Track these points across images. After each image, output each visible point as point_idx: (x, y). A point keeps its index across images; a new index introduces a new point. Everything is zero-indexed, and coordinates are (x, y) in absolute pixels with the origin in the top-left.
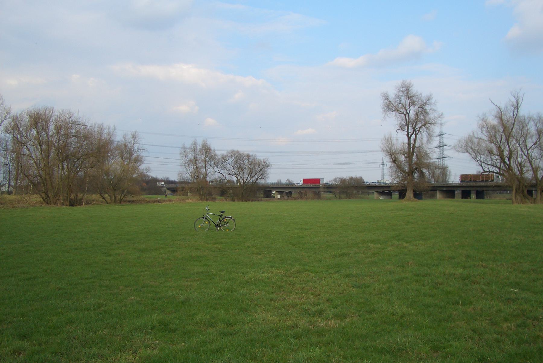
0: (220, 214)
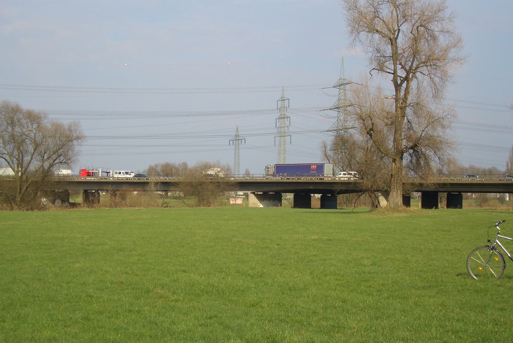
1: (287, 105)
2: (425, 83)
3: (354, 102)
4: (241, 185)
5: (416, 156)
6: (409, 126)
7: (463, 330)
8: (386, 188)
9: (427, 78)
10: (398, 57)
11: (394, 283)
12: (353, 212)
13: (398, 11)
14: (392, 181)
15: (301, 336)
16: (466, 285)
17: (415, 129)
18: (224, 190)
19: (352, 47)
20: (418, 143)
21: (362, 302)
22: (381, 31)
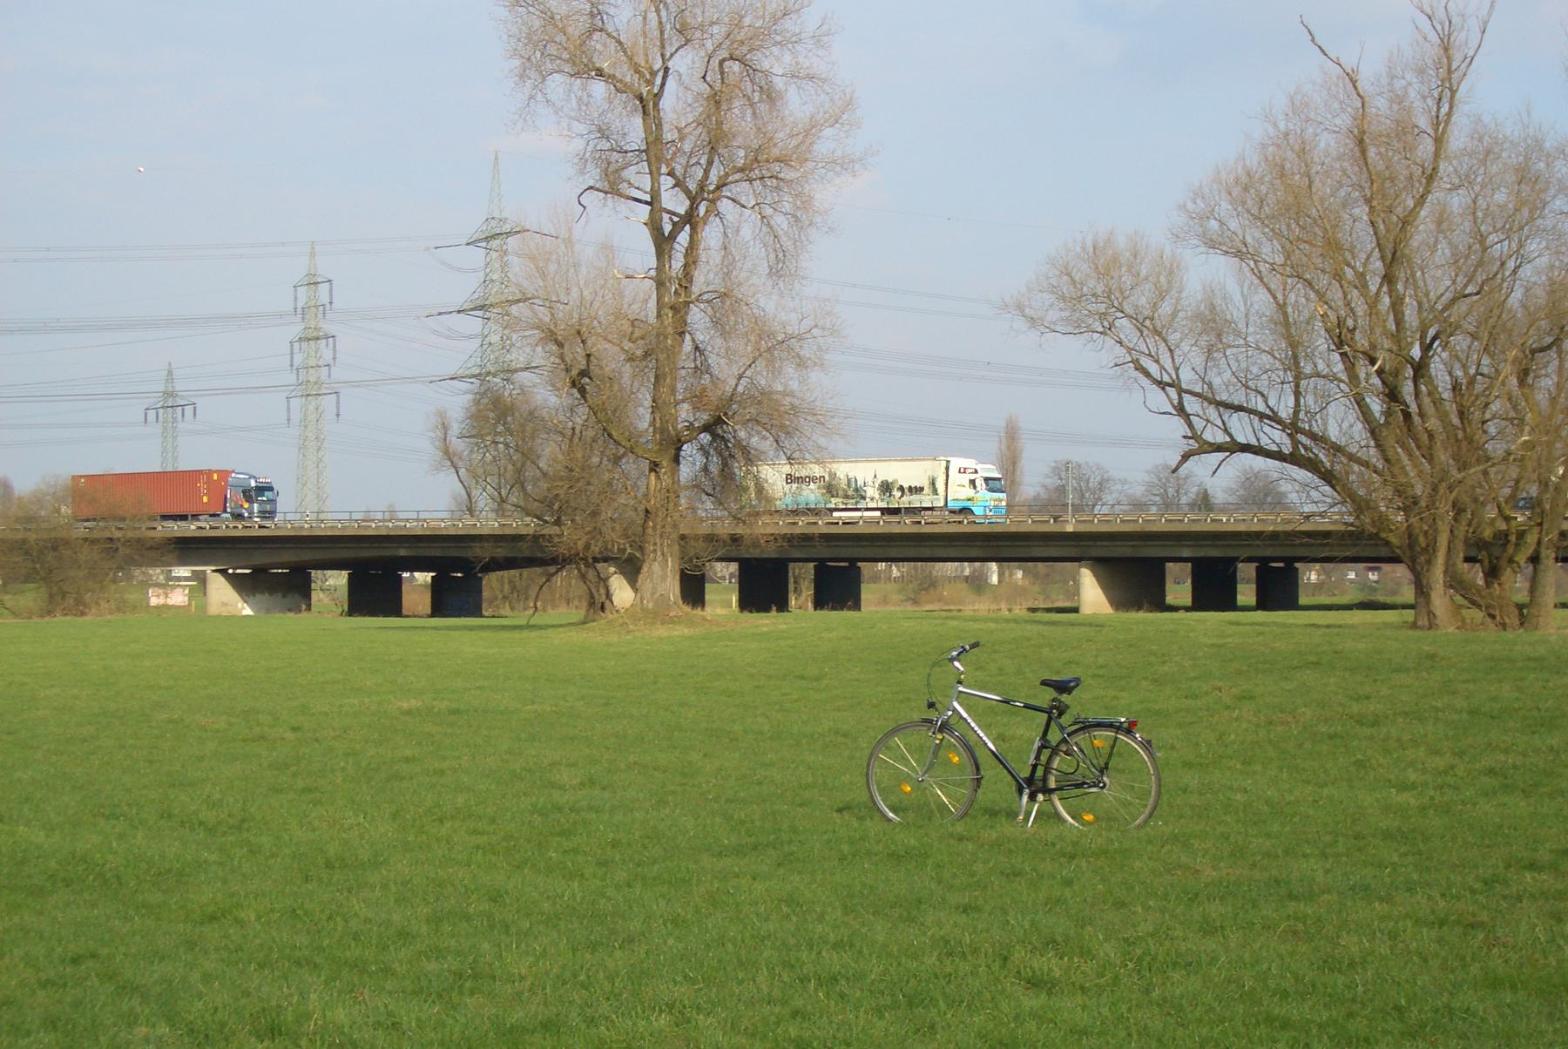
0: (1046, 697)
1: (324, 299)
2: (746, 232)
4: (181, 548)
5: (720, 454)
6: (698, 362)
8: (629, 551)
9: (752, 217)
10: (665, 152)
11: (648, 837)
12: (529, 627)
13: (664, 13)
14: (650, 531)
15: (357, 1007)
16: (864, 840)
17: (715, 371)
18: (131, 561)
20: (725, 414)
21: (548, 898)
22: (611, 72)
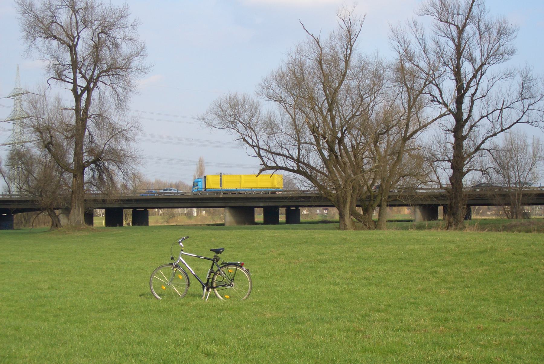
0: (212, 255)
2: (107, 94)
3: (31, 114)
6: (91, 139)
7: (143, 353)
8: (66, 205)
11: (72, 307)
13: (78, 17)
14: (74, 198)
17: (96, 142)
19: (28, 54)
20: (100, 157)
21: (36, 328)
